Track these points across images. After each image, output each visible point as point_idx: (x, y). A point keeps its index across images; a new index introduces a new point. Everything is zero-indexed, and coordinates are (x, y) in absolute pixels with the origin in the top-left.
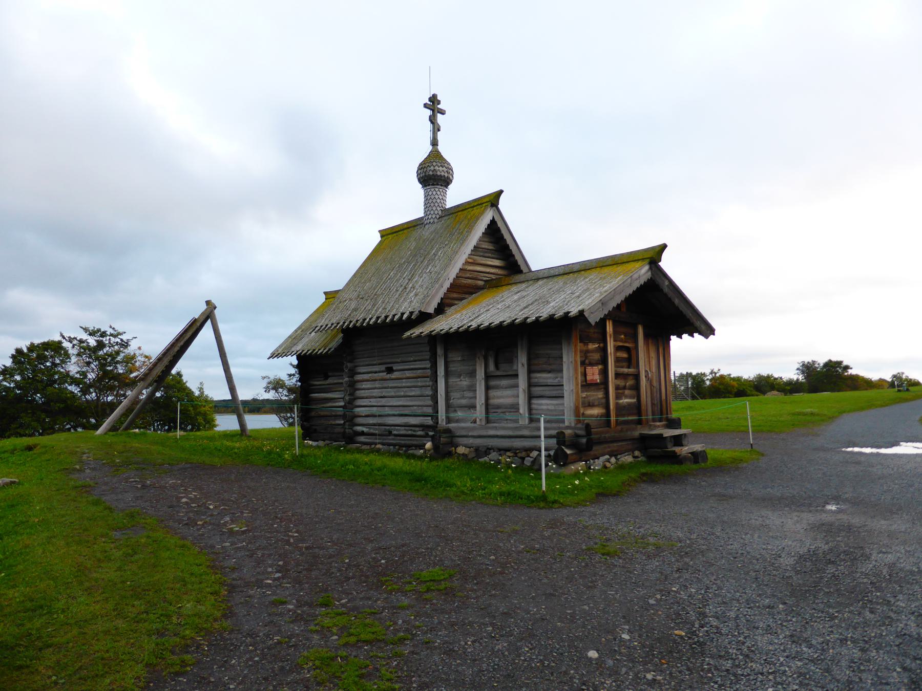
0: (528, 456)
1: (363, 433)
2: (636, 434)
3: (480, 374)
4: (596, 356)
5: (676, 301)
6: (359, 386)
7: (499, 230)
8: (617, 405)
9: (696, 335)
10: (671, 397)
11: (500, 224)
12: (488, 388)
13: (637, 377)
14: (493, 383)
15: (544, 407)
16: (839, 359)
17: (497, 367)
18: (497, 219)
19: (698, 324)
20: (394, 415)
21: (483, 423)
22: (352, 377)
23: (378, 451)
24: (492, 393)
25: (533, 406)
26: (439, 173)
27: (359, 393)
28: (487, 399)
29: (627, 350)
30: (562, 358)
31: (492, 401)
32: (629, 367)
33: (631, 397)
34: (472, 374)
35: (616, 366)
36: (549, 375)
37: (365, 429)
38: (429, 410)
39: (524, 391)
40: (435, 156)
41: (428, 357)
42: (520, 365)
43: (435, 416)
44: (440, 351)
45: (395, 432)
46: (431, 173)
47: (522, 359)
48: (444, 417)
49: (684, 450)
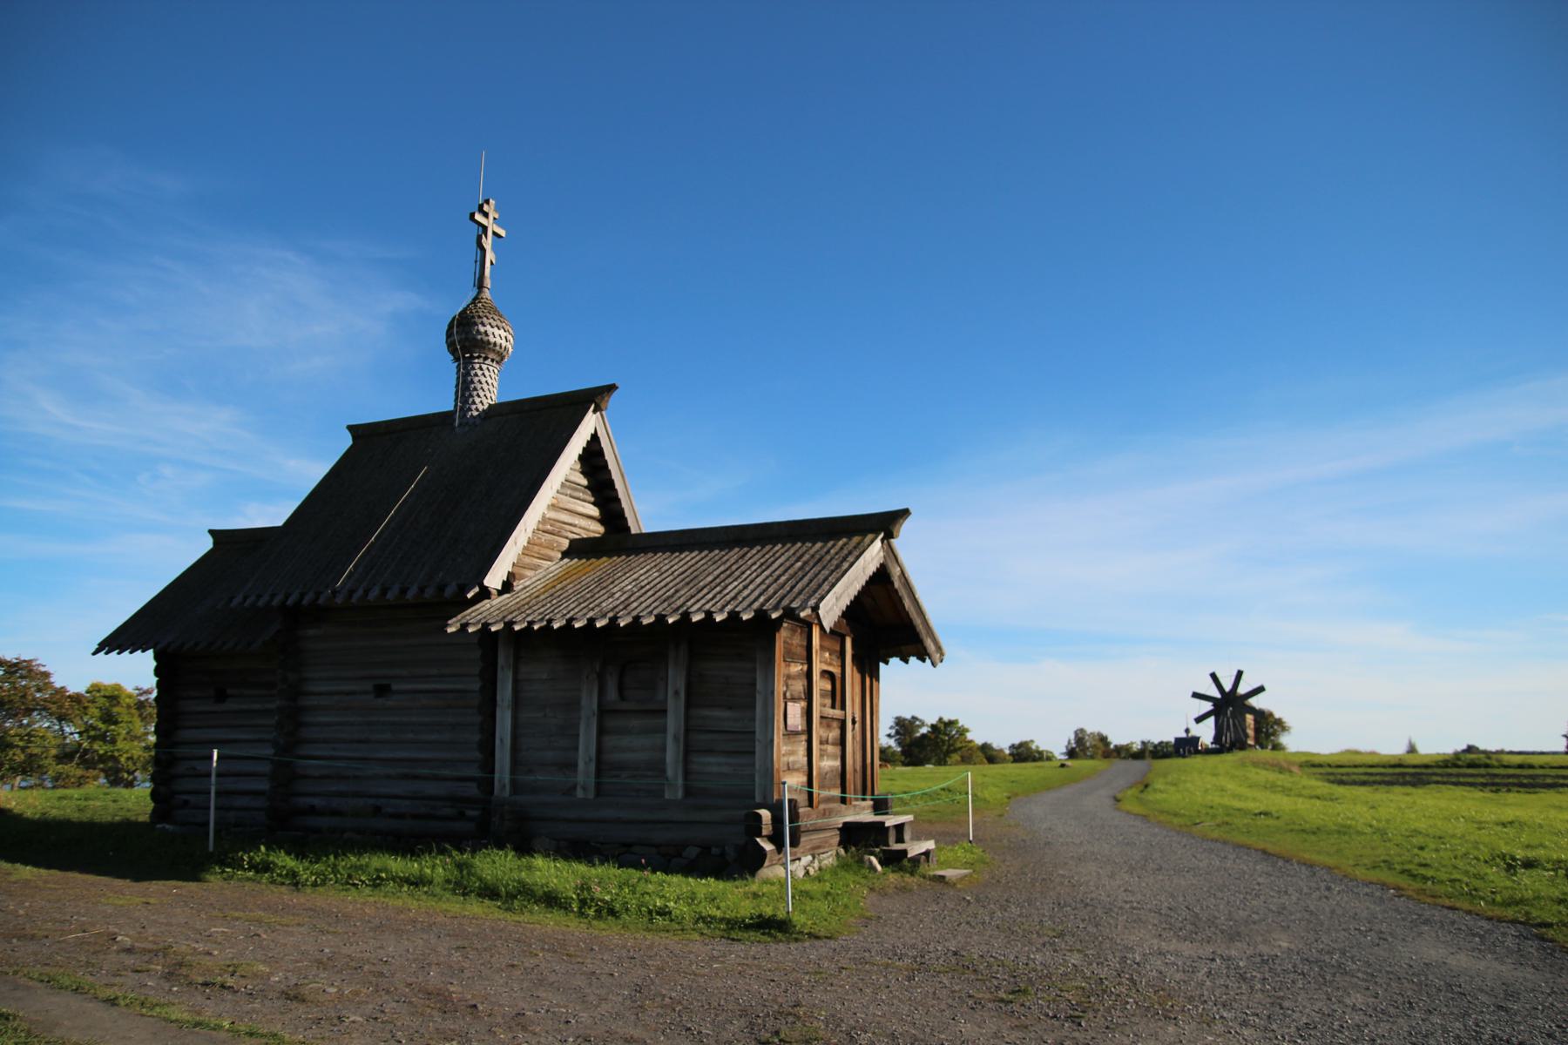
0: (680, 855)
1: (312, 810)
2: (840, 821)
3: (589, 702)
7: (601, 453)
9: (913, 660)
10: (877, 762)
12: (601, 731)
13: (843, 724)
15: (715, 769)
16: (953, 718)
17: (622, 697)
20: (388, 777)
21: (591, 795)
24: (610, 741)
26: (492, 340)
28: (599, 751)
30: (754, 685)
33: (833, 757)
34: (573, 705)
36: (726, 714)
37: (316, 802)
38: (473, 771)
39: (676, 738)
40: (476, 299)
43: (487, 784)
44: (502, 659)
47: (676, 680)
48: (507, 781)
49: (915, 848)
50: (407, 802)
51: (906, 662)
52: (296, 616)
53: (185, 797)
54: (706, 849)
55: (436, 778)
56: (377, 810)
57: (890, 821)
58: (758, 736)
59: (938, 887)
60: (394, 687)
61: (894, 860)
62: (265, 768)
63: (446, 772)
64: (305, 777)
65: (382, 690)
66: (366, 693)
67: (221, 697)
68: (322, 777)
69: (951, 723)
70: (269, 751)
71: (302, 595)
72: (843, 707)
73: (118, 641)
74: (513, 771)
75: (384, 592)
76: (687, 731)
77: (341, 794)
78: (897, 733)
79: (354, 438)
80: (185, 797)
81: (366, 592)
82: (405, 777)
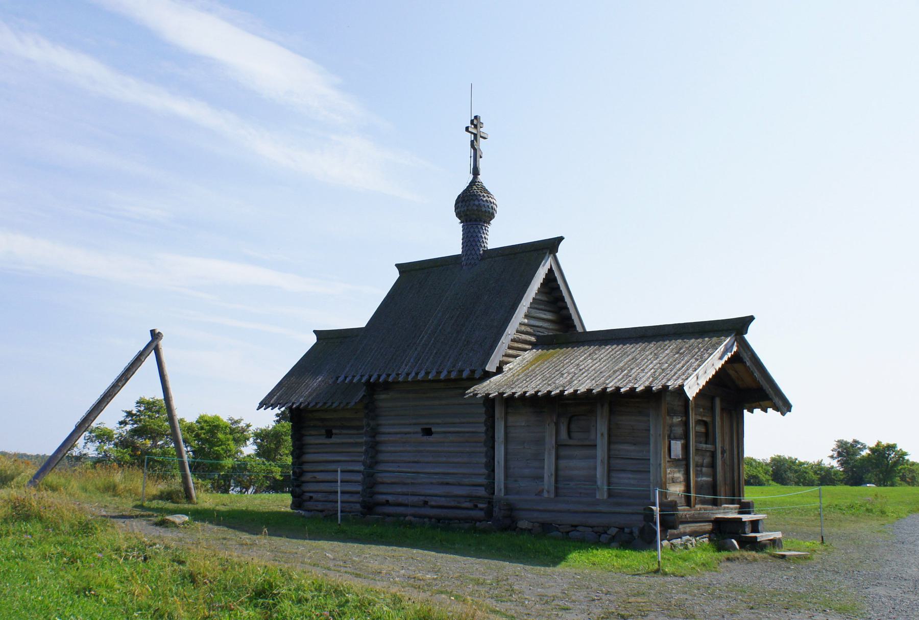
0: (605, 533)
1: (387, 503)
3: (550, 441)
4: (679, 430)
5: (757, 374)
6: (381, 467)
7: (555, 280)
8: (696, 482)
9: (770, 410)
11: (557, 274)
12: (558, 458)
13: (713, 455)
14: (563, 452)
16: (891, 443)
18: (554, 268)
19: (776, 400)
21: (552, 496)
22: (374, 437)
23: (411, 523)
24: (563, 463)
25: (614, 480)
27: (381, 457)
29: (705, 423)
31: (561, 473)
32: (706, 443)
33: (707, 476)
34: (540, 442)
35: (696, 442)
36: (632, 448)
37: (390, 498)
38: (482, 480)
40: (473, 183)
41: (483, 420)
42: (599, 435)
43: (491, 487)
45: (433, 503)
46: (475, 208)
47: (601, 427)
48: (502, 487)
49: (763, 536)
50: (443, 499)
51: (766, 412)
52: (373, 388)
53: (311, 495)
54: (622, 529)
55: (460, 485)
56: (426, 503)
57: (746, 518)
58: (651, 461)
59: (780, 561)
60: (433, 430)
61: (753, 545)
62: (360, 477)
63: (466, 481)
64: (383, 483)
65: (428, 432)
66: (416, 433)
67: (329, 434)
68: (392, 483)
69: (891, 447)
70: (362, 468)
71: (379, 376)
72: (714, 443)
73: (266, 403)
74: (507, 476)
75: (427, 373)
76: (609, 457)
77: (404, 494)
78: (839, 454)
79: (400, 273)
80: (311, 495)
81: (417, 374)
82: (442, 484)
